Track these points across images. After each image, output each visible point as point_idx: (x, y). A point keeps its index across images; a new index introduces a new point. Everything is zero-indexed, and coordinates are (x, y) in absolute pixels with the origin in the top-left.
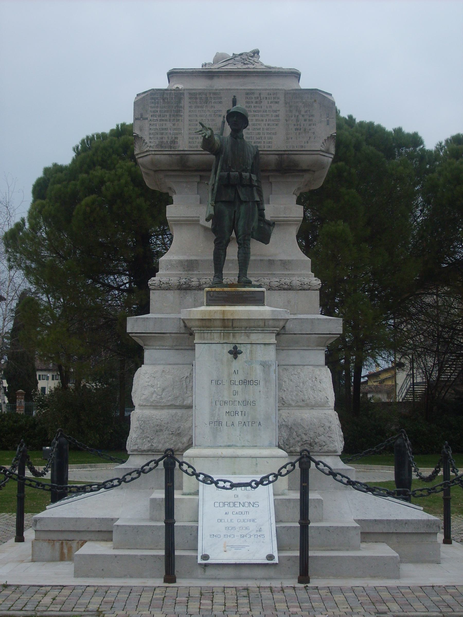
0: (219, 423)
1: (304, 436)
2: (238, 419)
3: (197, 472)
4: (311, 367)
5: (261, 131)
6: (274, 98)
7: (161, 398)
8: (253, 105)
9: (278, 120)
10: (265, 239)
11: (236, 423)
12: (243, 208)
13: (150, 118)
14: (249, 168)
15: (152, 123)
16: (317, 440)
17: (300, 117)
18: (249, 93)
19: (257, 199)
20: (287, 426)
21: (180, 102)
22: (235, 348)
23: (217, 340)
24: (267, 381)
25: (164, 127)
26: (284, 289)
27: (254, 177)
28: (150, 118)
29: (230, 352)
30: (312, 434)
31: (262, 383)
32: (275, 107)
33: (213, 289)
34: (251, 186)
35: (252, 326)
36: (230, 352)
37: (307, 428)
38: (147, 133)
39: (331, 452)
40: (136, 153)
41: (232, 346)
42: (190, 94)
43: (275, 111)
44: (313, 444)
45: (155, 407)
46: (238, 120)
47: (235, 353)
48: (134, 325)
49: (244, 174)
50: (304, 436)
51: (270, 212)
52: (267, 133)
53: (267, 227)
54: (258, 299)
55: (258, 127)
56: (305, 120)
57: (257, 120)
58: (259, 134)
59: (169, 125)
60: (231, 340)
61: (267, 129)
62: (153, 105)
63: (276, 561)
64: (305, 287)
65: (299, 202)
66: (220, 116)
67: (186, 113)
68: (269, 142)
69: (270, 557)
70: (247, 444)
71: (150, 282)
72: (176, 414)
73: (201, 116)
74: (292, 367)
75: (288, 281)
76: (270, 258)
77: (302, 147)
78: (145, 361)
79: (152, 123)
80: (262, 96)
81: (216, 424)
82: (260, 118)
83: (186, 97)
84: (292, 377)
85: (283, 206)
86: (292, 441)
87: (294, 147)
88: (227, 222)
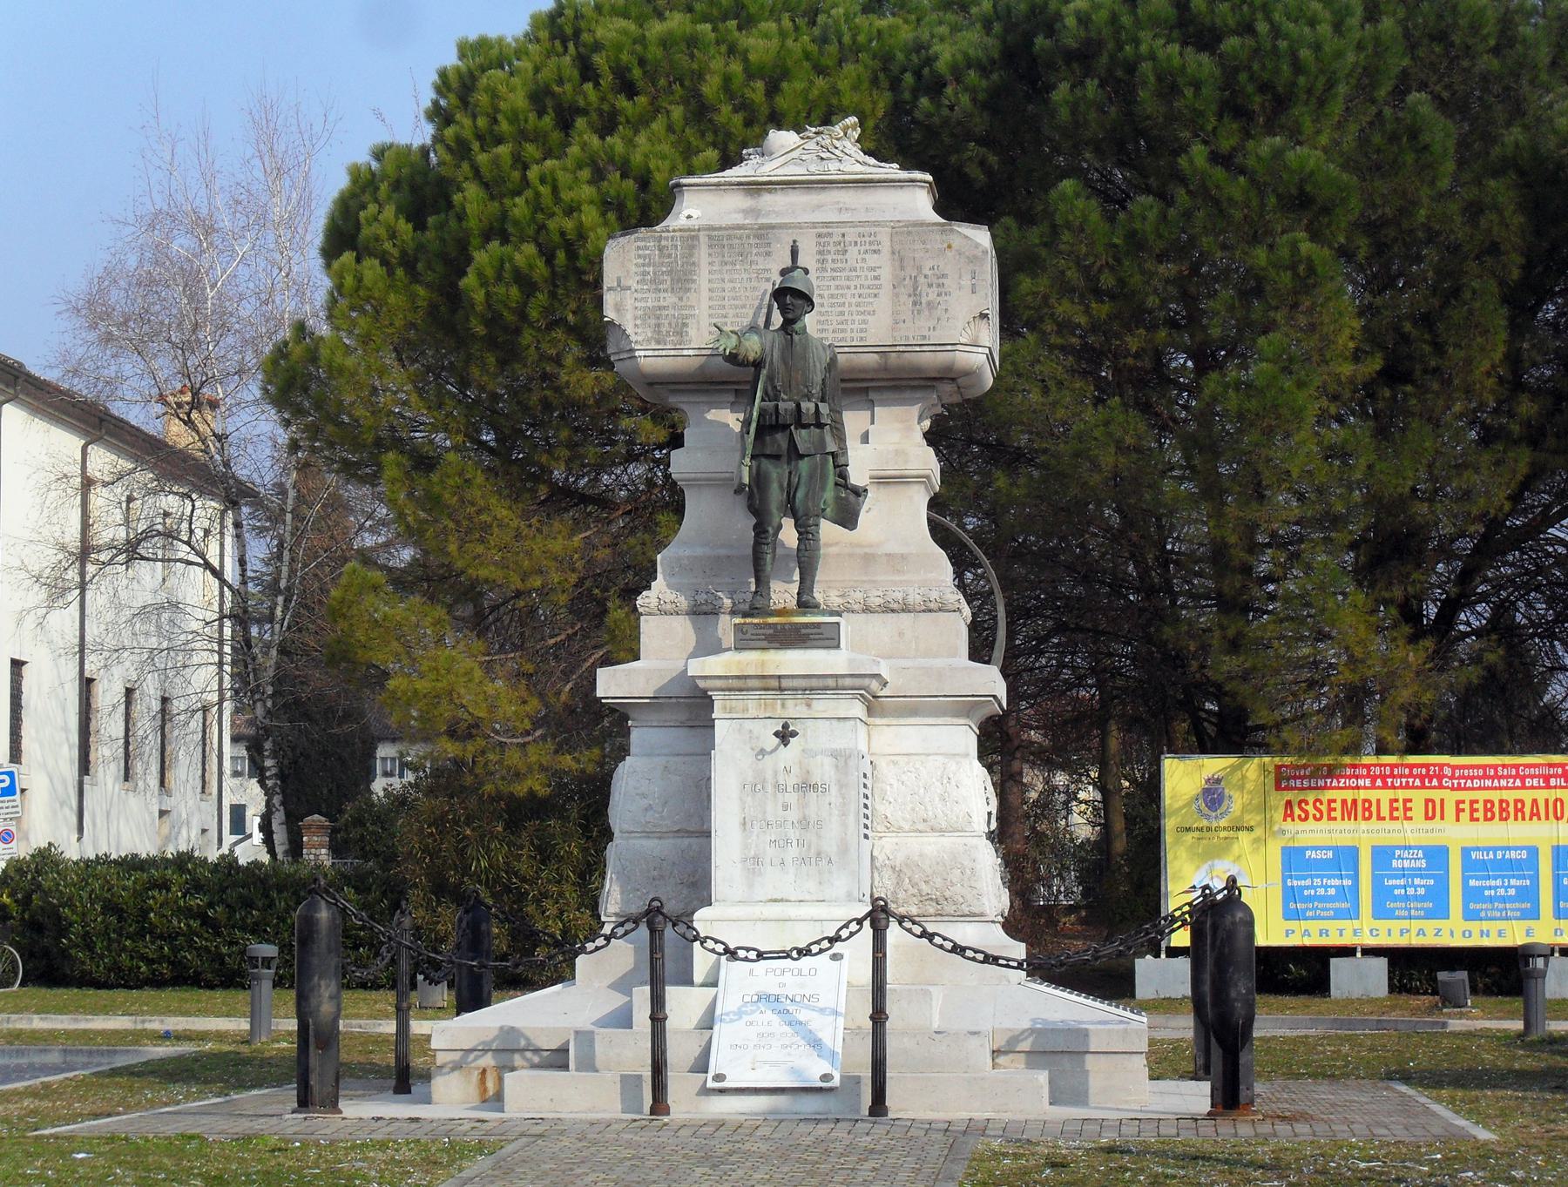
0: (757, 860)
1: (924, 887)
2: (793, 852)
3: (732, 947)
4: (940, 758)
5: (846, 309)
6: (871, 243)
7: (662, 818)
8: (829, 258)
9: (879, 287)
10: (847, 518)
11: (788, 861)
12: (804, 465)
13: (635, 286)
14: (816, 390)
15: (639, 296)
16: (947, 894)
17: (921, 280)
18: (823, 231)
19: (832, 447)
20: (893, 868)
21: (691, 255)
22: (785, 726)
23: (752, 713)
24: (842, 786)
25: (662, 303)
26: (893, 611)
27: (824, 409)
28: (635, 286)
29: (776, 734)
30: (938, 882)
31: (834, 790)
32: (872, 260)
33: (748, 620)
34: (820, 425)
35: (814, 686)
36: (776, 734)
37: (929, 871)
38: (629, 316)
39: (975, 915)
40: (609, 351)
41: (781, 722)
42: (710, 237)
43: (873, 269)
44: (941, 901)
45: (648, 834)
46: (791, 299)
47: (785, 736)
48: (612, 683)
49: (804, 405)
50: (924, 887)
51: (860, 466)
52: (859, 313)
53: (852, 497)
54: (827, 638)
55: (841, 300)
56: (930, 286)
57: (837, 287)
58: (842, 314)
59: (670, 299)
60: (779, 712)
61: (858, 305)
62: (641, 261)
63: (836, 1082)
64: (932, 606)
65: (932, 438)
66: (768, 280)
67: (703, 278)
68: (861, 331)
69: (826, 1077)
70: (807, 897)
71: (639, 601)
72: (690, 845)
73: (731, 281)
74: (905, 759)
75: (899, 596)
76: (867, 550)
77: (924, 337)
78: (633, 749)
79: (639, 296)
80: (847, 239)
81: (754, 863)
82: (844, 283)
83: (703, 238)
84: (904, 778)
85: (889, 449)
86: (901, 895)
87: (907, 338)
88: (776, 495)
